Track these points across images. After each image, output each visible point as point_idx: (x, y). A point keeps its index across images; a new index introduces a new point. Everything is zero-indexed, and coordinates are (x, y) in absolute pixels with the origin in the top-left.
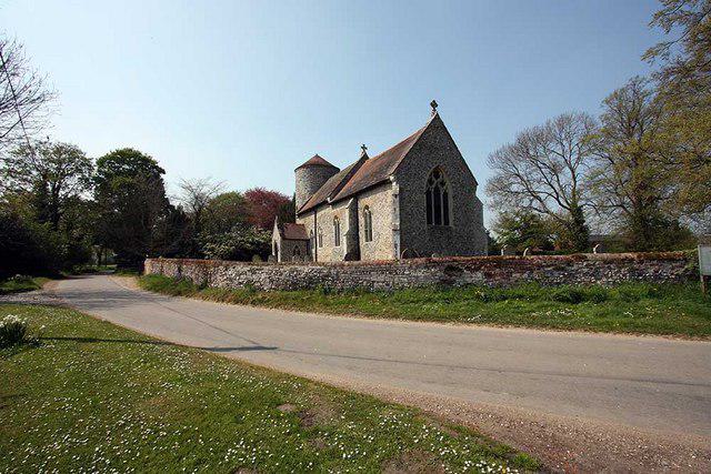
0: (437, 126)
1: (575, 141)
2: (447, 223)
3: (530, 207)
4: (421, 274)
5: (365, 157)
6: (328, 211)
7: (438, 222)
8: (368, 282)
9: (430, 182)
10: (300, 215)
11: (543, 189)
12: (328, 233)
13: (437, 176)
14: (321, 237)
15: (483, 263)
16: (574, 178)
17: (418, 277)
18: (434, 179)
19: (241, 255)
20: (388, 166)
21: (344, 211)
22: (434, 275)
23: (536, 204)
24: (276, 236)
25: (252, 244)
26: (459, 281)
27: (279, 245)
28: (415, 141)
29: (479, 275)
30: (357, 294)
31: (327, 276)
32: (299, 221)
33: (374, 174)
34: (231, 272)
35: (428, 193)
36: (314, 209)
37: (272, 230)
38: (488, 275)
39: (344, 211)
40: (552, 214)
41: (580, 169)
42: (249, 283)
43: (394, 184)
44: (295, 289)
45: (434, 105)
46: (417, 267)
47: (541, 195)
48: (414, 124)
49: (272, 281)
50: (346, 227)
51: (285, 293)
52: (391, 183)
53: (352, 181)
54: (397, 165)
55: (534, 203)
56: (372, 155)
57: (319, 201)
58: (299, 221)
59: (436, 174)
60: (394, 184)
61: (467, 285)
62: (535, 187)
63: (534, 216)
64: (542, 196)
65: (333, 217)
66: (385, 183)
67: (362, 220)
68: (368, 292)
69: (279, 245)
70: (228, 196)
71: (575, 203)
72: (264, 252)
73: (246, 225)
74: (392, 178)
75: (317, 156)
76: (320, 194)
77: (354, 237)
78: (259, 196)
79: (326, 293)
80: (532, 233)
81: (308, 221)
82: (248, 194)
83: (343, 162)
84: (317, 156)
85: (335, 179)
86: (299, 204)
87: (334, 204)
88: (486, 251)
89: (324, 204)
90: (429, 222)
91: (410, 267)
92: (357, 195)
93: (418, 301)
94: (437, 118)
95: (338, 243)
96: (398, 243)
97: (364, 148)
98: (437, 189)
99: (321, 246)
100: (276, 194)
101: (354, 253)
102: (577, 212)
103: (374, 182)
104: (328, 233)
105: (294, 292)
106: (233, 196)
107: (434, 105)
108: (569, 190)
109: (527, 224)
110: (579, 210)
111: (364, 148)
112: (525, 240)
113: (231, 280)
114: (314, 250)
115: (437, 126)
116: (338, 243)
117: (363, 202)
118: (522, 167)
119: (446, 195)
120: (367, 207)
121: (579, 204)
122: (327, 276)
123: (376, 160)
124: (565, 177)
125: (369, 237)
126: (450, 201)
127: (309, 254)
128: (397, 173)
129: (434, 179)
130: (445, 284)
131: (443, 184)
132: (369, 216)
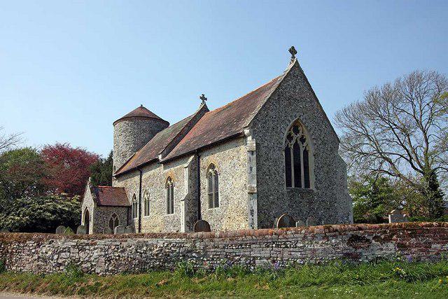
0: (296, 74)
1: (427, 99)
2: (307, 185)
3: (381, 170)
4: (318, 246)
5: (204, 110)
6: (160, 172)
7: (298, 184)
8: (248, 257)
9: (289, 137)
10: (118, 177)
11: (394, 150)
12: (157, 198)
13: (296, 131)
14: (147, 202)
15: (394, 231)
16: (427, 140)
17: (315, 250)
18: (293, 134)
19: (42, 226)
20: (240, 118)
21: (181, 172)
22: (335, 246)
23: (386, 166)
24: (88, 201)
25: (53, 212)
26: (367, 255)
27: (92, 213)
28: (273, 90)
29: (391, 246)
30: (234, 276)
31: (191, 252)
32: (116, 184)
33: (220, 128)
34: (46, 249)
35: (287, 150)
36: (140, 169)
37: (82, 193)
38: (401, 246)
39: (181, 172)
40: (404, 178)
41: (432, 131)
42: (74, 264)
43: (249, 138)
44: (144, 271)
45: (293, 51)
46: (314, 237)
47: (390, 157)
48: (275, 70)
49: (109, 260)
50: (183, 189)
51: (130, 277)
52: (245, 137)
53: (182, 142)
54: (252, 117)
55: (384, 165)
56: (212, 106)
57: (146, 160)
58: (116, 184)
59: (296, 128)
60: (249, 138)
61: (377, 259)
62: (385, 148)
63: (384, 180)
64: (394, 158)
65: (164, 179)
66: (237, 138)
67: (205, 182)
68: (248, 272)
69: (92, 213)
70: (21, 153)
71: (428, 165)
72: (71, 221)
73: (41, 189)
74: (247, 131)
75: (142, 107)
76: (146, 152)
77: (194, 202)
78: (61, 154)
79: (190, 274)
80: (382, 199)
81: (131, 185)
82: (45, 151)
83: (175, 112)
84: (142, 107)
85: (164, 136)
86: (117, 164)
87: (167, 163)
88: (351, 218)
89: (153, 162)
90: (289, 184)
91: (305, 238)
92: (198, 153)
93: (321, 283)
94: (297, 66)
95: (170, 209)
96: (255, 208)
97: (203, 98)
98: (296, 146)
99: (147, 213)
100: (83, 152)
101: (196, 221)
102: (431, 176)
103: (222, 136)
104: (157, 198)
105: (141, 275)
106: (28, 153)
107: (293, 51)
108: (420, 153)
109: (376, 191)
110: (433, 174)
111: (203, 98)
112: (375, 206)
113: (45, 260)
114: (136, 220)
115: (296, 74)
116: (170, 209)
117: (206, 160)
118: (370, 125)
119: (306, 152)
120: (212, 166)
121: (433, 167)
122: (191, 252)
123: (219, 112)
124: (417, 137)
125: (214, 201)
126: (311, 159)
127: (129, 222)
128: (253, 125)
129: (293, 134)
130: (351, 258)
131: (303, 140)
132: (214, 178)
